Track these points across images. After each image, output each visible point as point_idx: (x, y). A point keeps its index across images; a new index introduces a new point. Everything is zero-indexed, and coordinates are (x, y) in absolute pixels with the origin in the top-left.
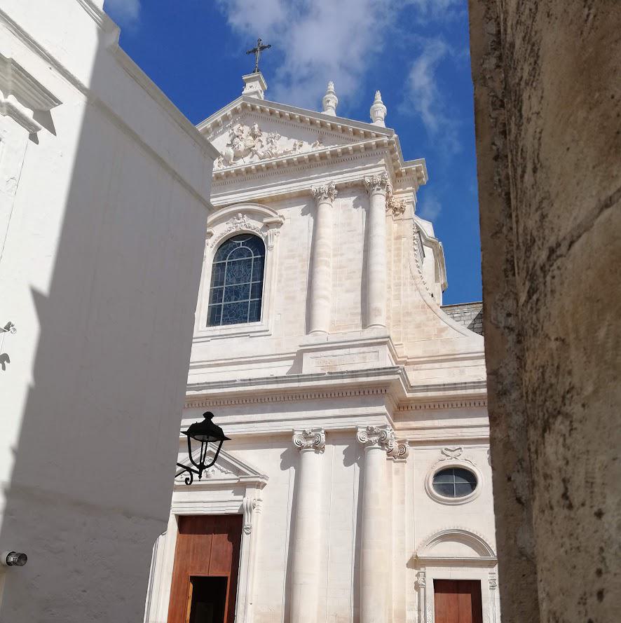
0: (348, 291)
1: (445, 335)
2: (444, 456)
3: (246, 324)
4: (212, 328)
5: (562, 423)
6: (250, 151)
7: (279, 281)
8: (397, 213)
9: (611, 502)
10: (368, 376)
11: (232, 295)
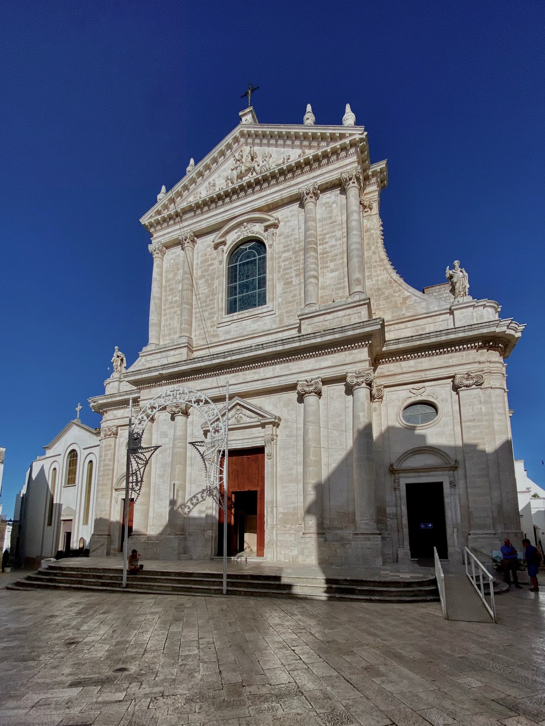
0: (332, 271)
2: (412, 395)
3: (256, 308)
4: (231, 315)
5: (498, 395)
6: (250, 170)
7: (279, 272)
8: (366, 210)
11: (244, 289)
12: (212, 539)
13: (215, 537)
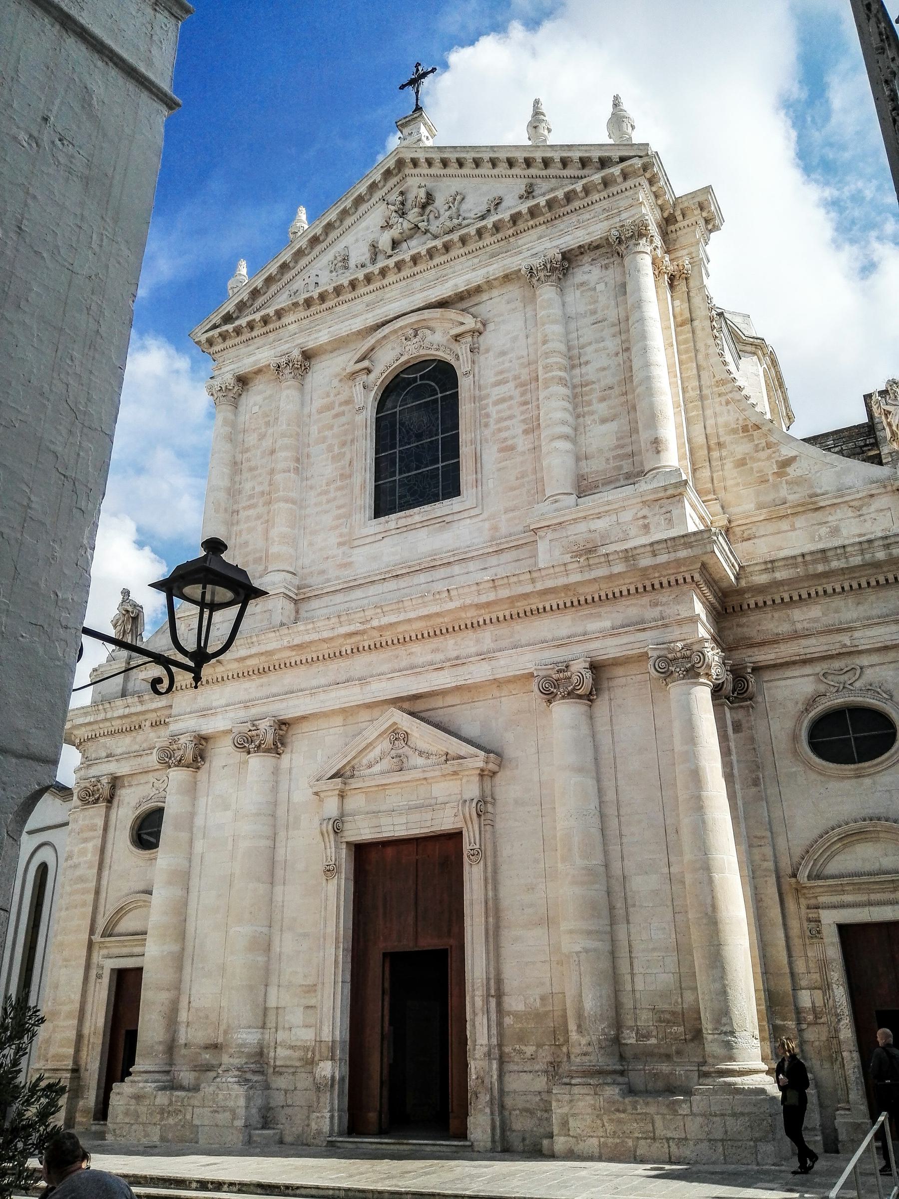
0: (603, 421)
1: (793, 471)
3: (438, 505)
9: (1, 899)
10: (497, 1012)
12: (332, 1086)
13: (342, 1079)
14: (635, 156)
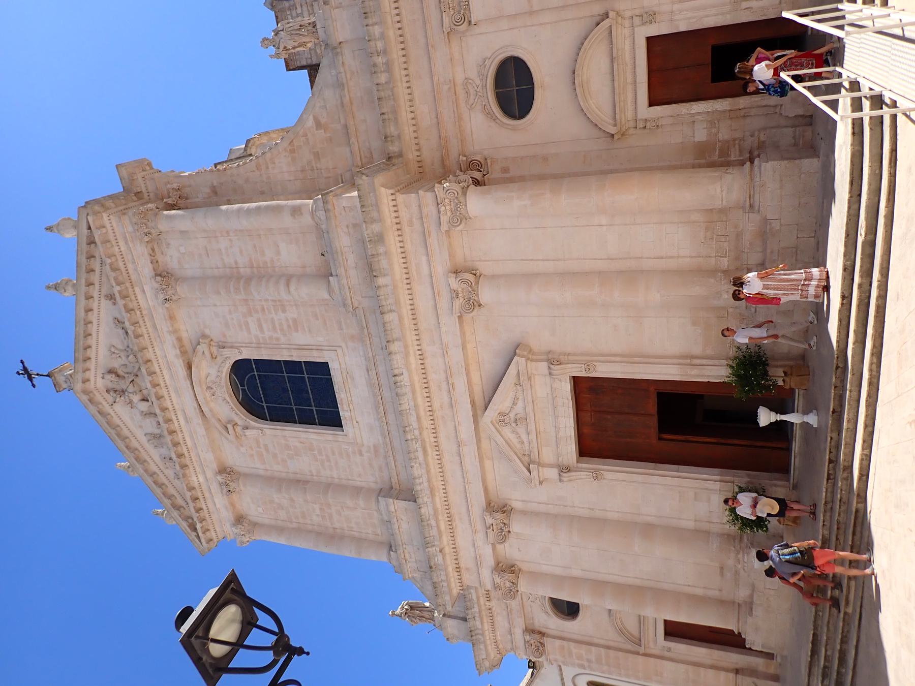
14: (87, 218)
